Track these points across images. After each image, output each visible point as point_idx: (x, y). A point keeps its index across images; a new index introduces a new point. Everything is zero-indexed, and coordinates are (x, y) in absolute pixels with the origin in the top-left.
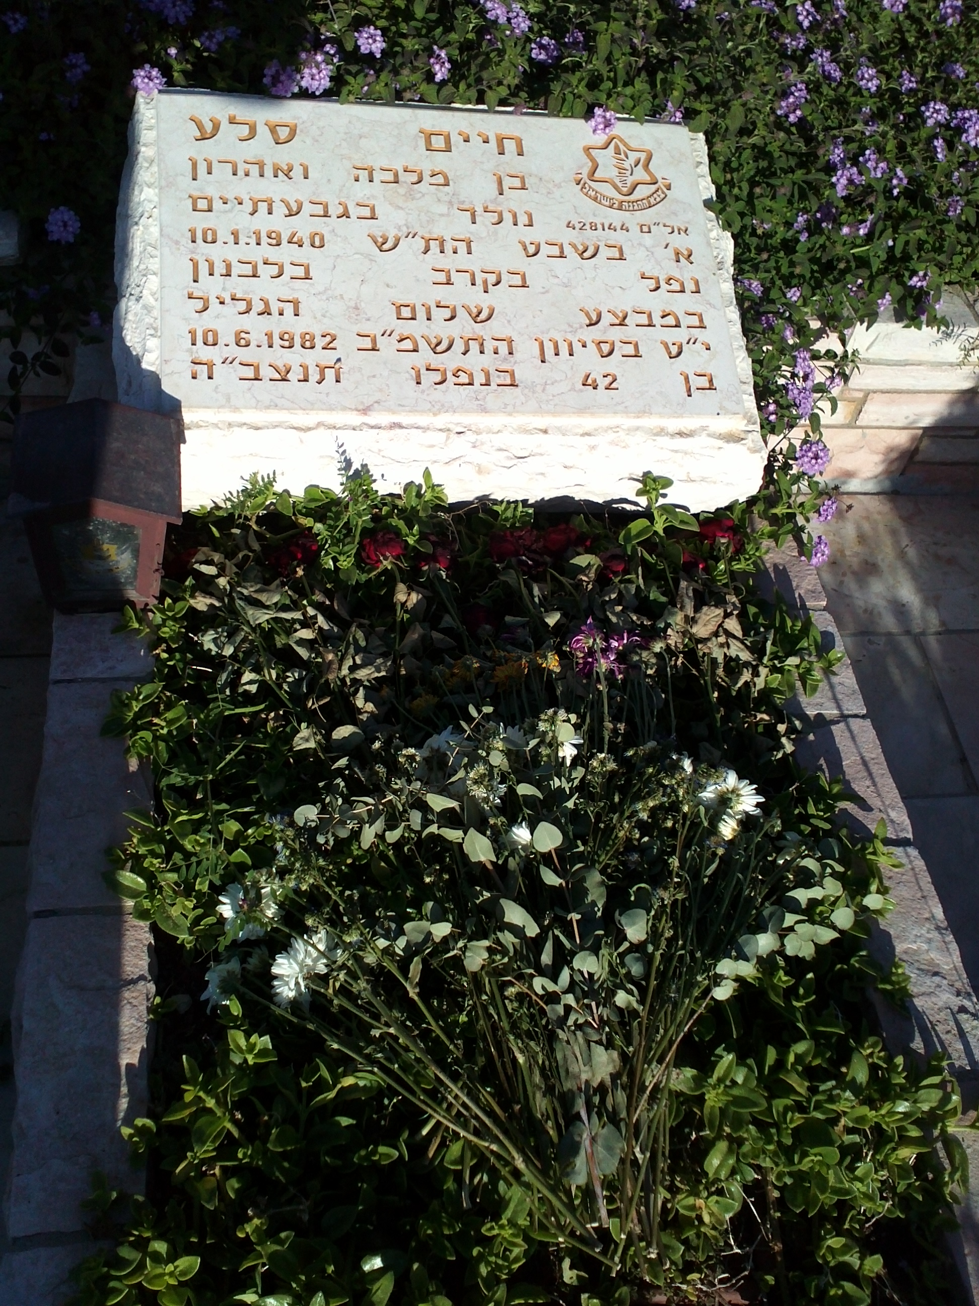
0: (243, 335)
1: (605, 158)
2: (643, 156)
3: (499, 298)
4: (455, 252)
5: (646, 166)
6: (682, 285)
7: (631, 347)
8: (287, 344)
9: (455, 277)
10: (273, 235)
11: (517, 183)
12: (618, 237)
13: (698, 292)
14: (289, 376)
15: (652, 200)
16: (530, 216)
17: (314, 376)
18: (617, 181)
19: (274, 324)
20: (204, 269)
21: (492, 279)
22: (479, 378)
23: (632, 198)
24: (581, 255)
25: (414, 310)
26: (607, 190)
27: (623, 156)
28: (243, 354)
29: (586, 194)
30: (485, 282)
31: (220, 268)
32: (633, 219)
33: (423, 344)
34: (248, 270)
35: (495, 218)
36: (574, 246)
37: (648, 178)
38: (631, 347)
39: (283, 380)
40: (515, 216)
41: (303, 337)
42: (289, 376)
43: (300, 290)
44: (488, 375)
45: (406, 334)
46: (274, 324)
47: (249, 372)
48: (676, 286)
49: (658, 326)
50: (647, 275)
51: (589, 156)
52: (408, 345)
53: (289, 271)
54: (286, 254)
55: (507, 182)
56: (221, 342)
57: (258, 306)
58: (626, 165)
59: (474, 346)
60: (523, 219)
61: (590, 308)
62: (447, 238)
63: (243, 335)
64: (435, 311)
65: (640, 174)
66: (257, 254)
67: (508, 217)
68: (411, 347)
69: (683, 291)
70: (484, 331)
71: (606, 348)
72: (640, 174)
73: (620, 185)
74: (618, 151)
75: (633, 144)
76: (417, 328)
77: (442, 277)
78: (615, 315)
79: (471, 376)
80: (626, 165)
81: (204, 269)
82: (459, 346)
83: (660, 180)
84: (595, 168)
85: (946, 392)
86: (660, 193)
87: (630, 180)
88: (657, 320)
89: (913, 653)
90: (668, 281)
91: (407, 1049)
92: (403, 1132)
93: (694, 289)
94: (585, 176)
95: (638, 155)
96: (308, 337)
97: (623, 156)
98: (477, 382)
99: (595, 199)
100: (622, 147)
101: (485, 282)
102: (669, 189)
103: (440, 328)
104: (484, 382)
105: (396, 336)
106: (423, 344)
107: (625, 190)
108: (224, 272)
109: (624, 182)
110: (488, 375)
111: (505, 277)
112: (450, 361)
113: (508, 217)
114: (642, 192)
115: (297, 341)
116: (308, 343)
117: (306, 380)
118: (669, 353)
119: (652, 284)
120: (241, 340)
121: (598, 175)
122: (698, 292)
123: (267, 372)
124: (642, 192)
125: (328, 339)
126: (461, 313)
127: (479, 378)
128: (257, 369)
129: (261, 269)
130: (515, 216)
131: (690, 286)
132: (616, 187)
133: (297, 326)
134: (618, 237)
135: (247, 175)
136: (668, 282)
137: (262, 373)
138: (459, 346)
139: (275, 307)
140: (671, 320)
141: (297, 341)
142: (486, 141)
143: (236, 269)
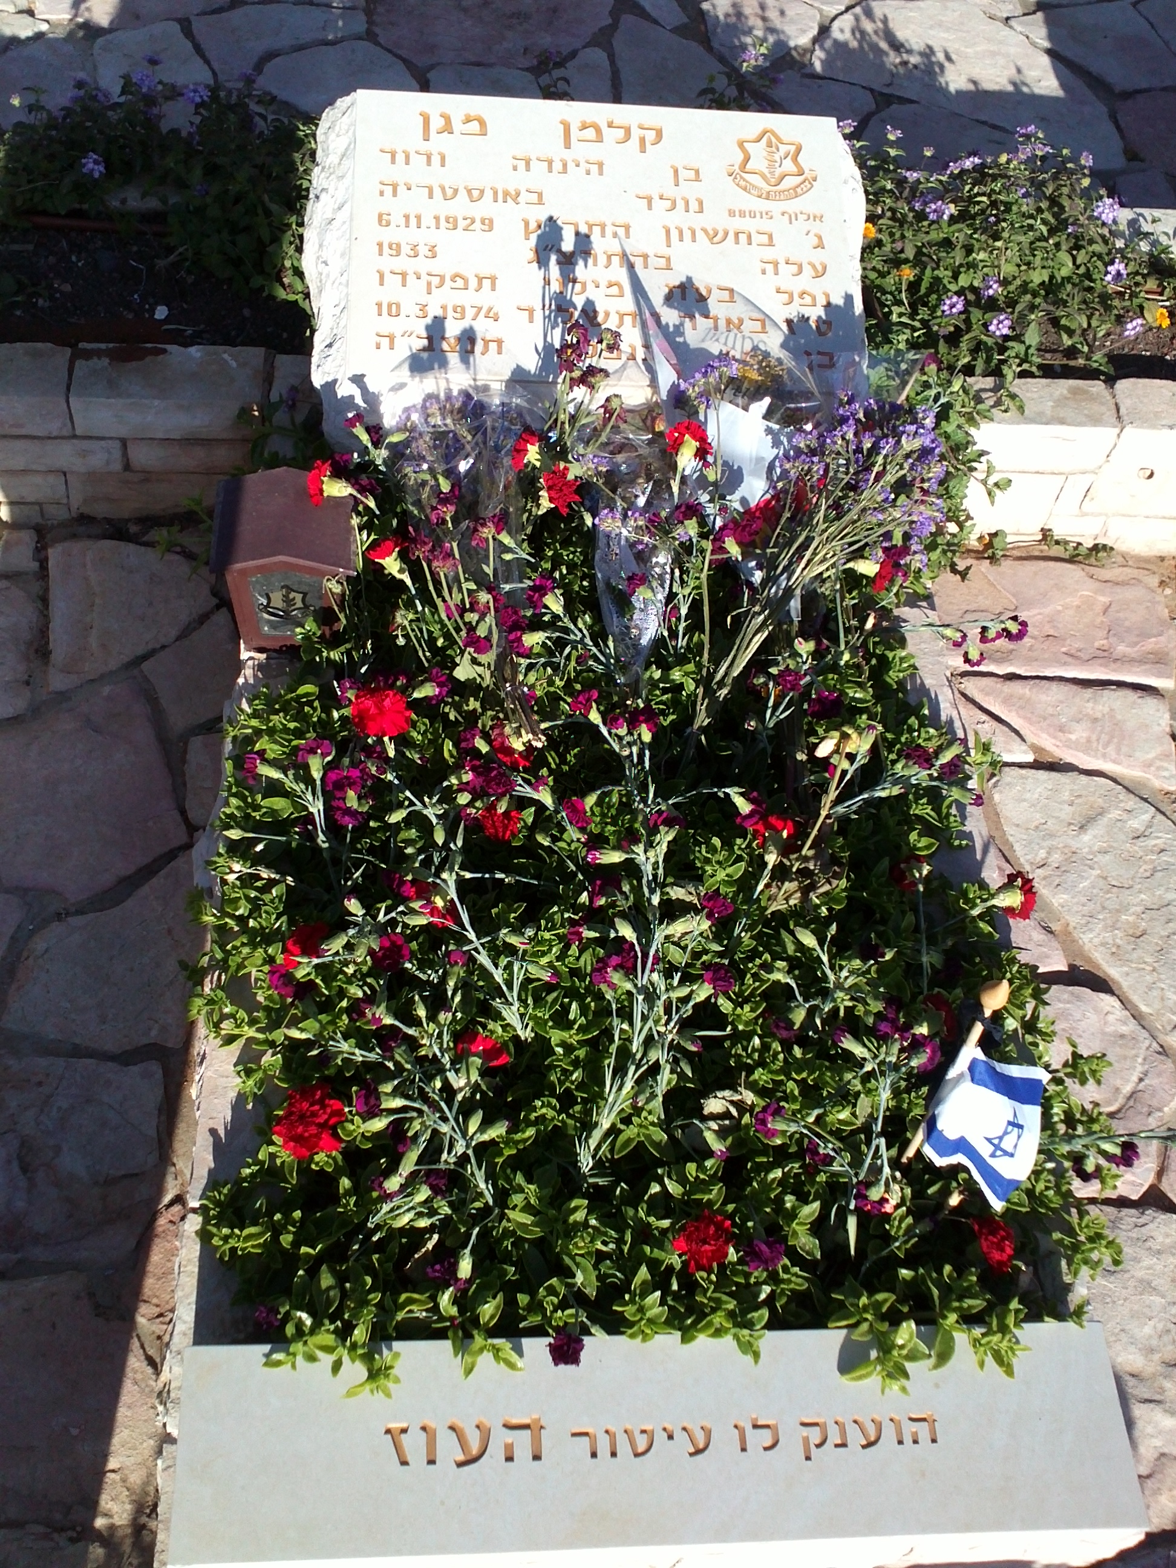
1: (758, 151)
2: (793, 148)
5: (795, 160)
8: (458, 316)
12: (766, 225)
15: (799, 190)
16: (701, 203)
18: (766, 171)
24: (711, 239)
32: (776, 207)
35: (668, 204)
36: (705, 231)
40: (687, 203)
41: (390, 306)
55: (683, 174)
56: (403, 313)
58: (777, 157)
60: (694, 206)
67: (680, 204)
72: (788, 166)
74: (769, 144)
75: (785, 139)
80: (777, 157)
83: (807, 171)
84: (747, 159)
85: (403, 362)
87: (778, 172)
90: (802, 295)
91: (59, 1109)
92: (1059, 1265)
94: (736, 167)
99: (745, 189)
100: (773, 140)
113: (680, 204)
114: (789, 182)
121: (749, 167)
124: (789, 182)
130: (687, 203)
134: (766, 225)
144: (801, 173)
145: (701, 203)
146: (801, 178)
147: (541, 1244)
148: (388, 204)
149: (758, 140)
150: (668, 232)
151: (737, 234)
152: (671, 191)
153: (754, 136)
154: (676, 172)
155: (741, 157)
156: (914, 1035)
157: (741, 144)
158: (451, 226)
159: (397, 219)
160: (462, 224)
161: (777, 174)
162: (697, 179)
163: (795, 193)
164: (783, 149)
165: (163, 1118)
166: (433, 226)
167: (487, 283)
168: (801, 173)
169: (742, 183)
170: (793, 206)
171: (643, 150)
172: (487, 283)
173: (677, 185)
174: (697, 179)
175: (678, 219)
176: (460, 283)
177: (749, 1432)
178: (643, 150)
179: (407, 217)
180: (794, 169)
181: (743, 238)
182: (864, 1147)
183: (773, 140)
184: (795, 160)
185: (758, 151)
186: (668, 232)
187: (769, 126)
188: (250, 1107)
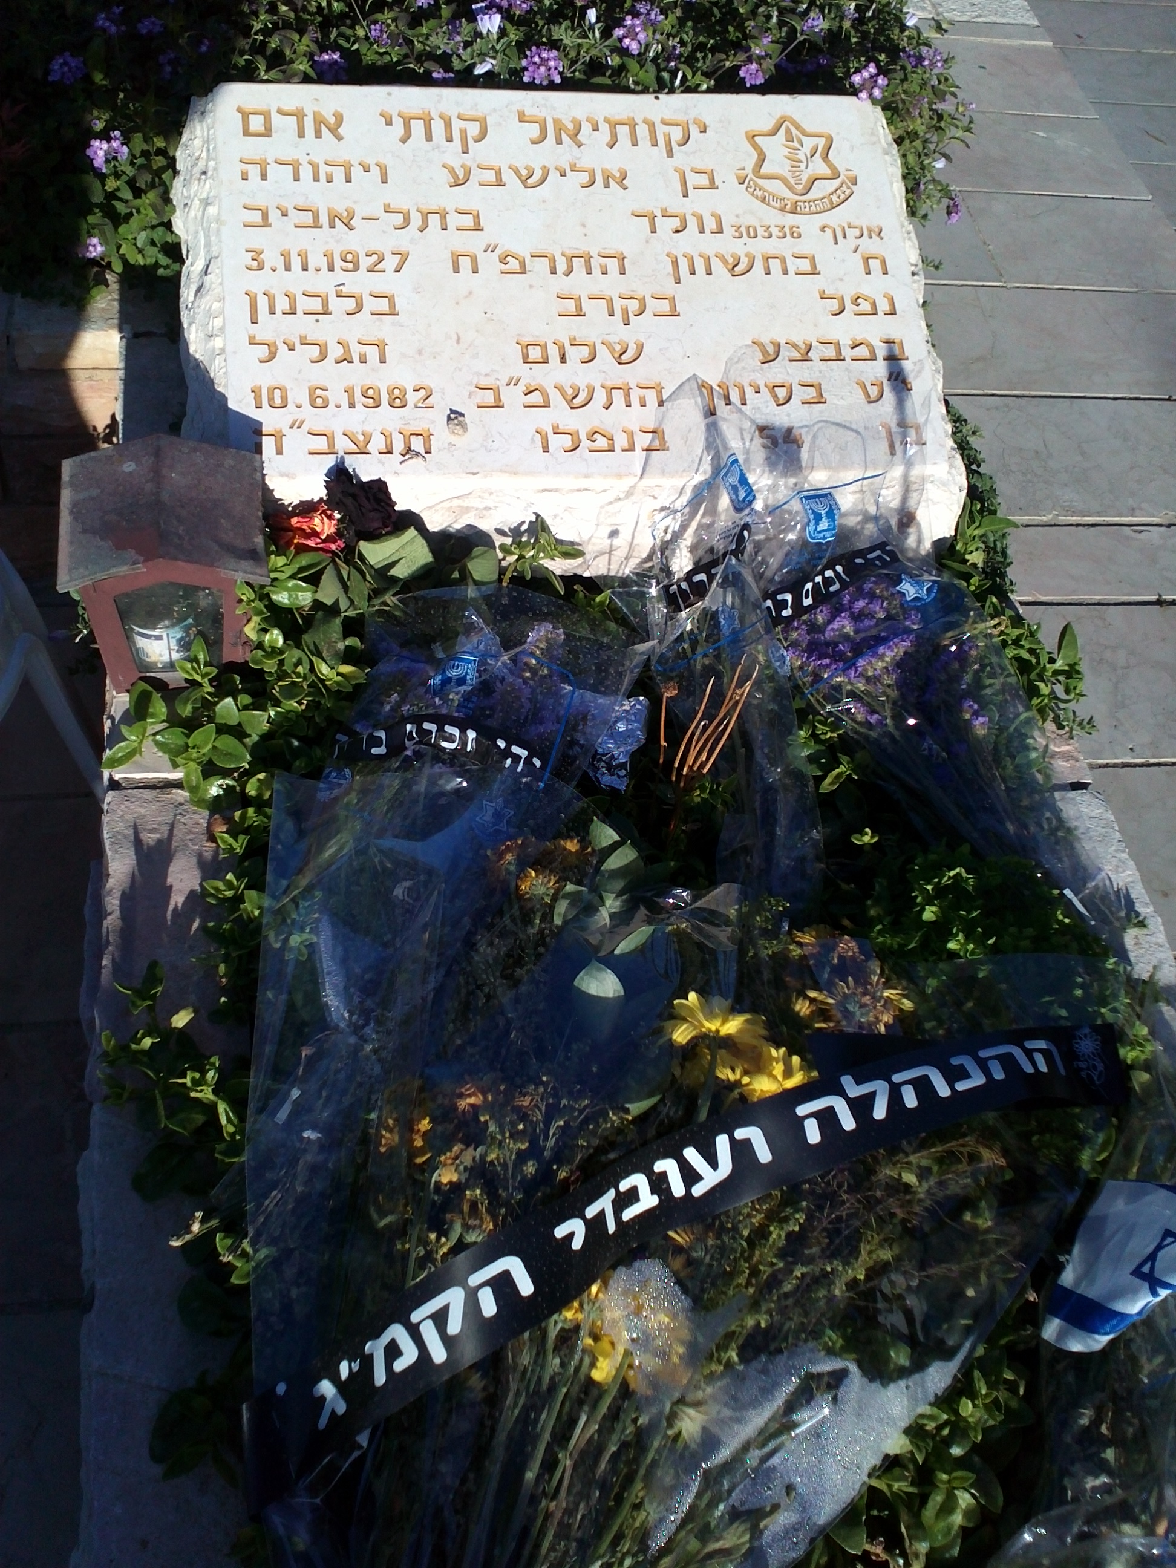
0: (319, 392)
2: (821, 142)
3: (644, 328)
4: (605, 273)
5: (825, 157)
6: (874, 304)
9: (586, 305)
10: (349, 257)
11: (704, 180)
19: (356, 375)
20: (263, 303)
21: (634, 306)
22: (621, 441)
23: (810, 196)
25: (544, 348)
26: (775, 187)
27: (796, 144)
28: (316, 419)
29: (753, 194)
30: (625, 311)
31: (282, 304)
32: (809, 224)
33: (555, 397)
34: (316, 304)
37: (827, 172)
41: (390, 392)
43: (384, 329)
44: (631, 435)
46: (356, 375)
48: (865, 306)
49: (848, 359)
50: (828, 293)
51: (755, 146)
52: (536, 398)
53: (370, 304)
54: (360, 282)
55: (692, 180)
57: (336, 352)
59: (618, 396)
60: (710, 224)
61: (765, 339)
62: (594, 254)
63: (319, 392)
64: (571, 352)
65: (819, 167)
66: (325, 283)
67: (692, 224)
70: (631, 375)
71: (782, 393)
72: (819, 167)
73: (792, 181)
74: (790, 138)
75: (809, 128)
76: (552, 375)
77: (570, 305)
78: (795, 346)
81: (263, 303)
82: (600, 397)
83: (842, 170)
84: (762, 159)
86: (844, 188)
88: (847, 352)
89: (389, 815)
90: (856, 301)
94: (749, 170)
95: (816, 140)
96: (397, 392)
97: (796, 144)
98: (617, 448)
99: (763, 200)
100: (793, 129)
101: (625, 311)
102: (855, 184)
103: (575, 374)
104: (626, 446)
105: (521, 387)
106: (555, 397)
107: (799, 188)
108: (287, 308)
109: (798, 179)
110: (631, 435)
111: (651, 303)
112: (592, 416)
113: (692, 224)
114: (821, 189)
115: (385, 398)
116: (398, 401)
118: (867, 395)
119: (835, 305)
120: (317, 399)
121: (764, 170)
124: (821, 189)
125: (422, 393)
126: (603, 352)
129: (334, 303)
131: (883, 306)
133: (384, 379)
135: (330, 180)
136: (856, 301)
138: (600, 397)
139: (356, 350)
140: (862, 351)
141: (385, 398)
143: (303, 304)
144: (836, 175)
146: (836, 183)
147: (693, 1455)
148: (258, 238)
149: (774, 132)
150: (675, 263)
151: (766, 259)
152: (677, 204)
153: (768, 126)
157: (752, 137)
158: (350, 266)
159: (272, 258)
160: (365, 262)
161: (805, 178)
162: (713, 186)
164: (809, 143)
165: (761, 1439)
166: (281, 267)
168: (836, 175)
169: (759, 193)
171: (670, 154)
173: (686, 196)
174: (713, 186)
175: (691, 243)
178: (670, 154)
179: (286, 256)
180: (827, 172)
181: (775, 265)
183: (793, 129)
184: (825, 157)
185: (775, 148)
186: (675, 263)
188: (176, 1243)
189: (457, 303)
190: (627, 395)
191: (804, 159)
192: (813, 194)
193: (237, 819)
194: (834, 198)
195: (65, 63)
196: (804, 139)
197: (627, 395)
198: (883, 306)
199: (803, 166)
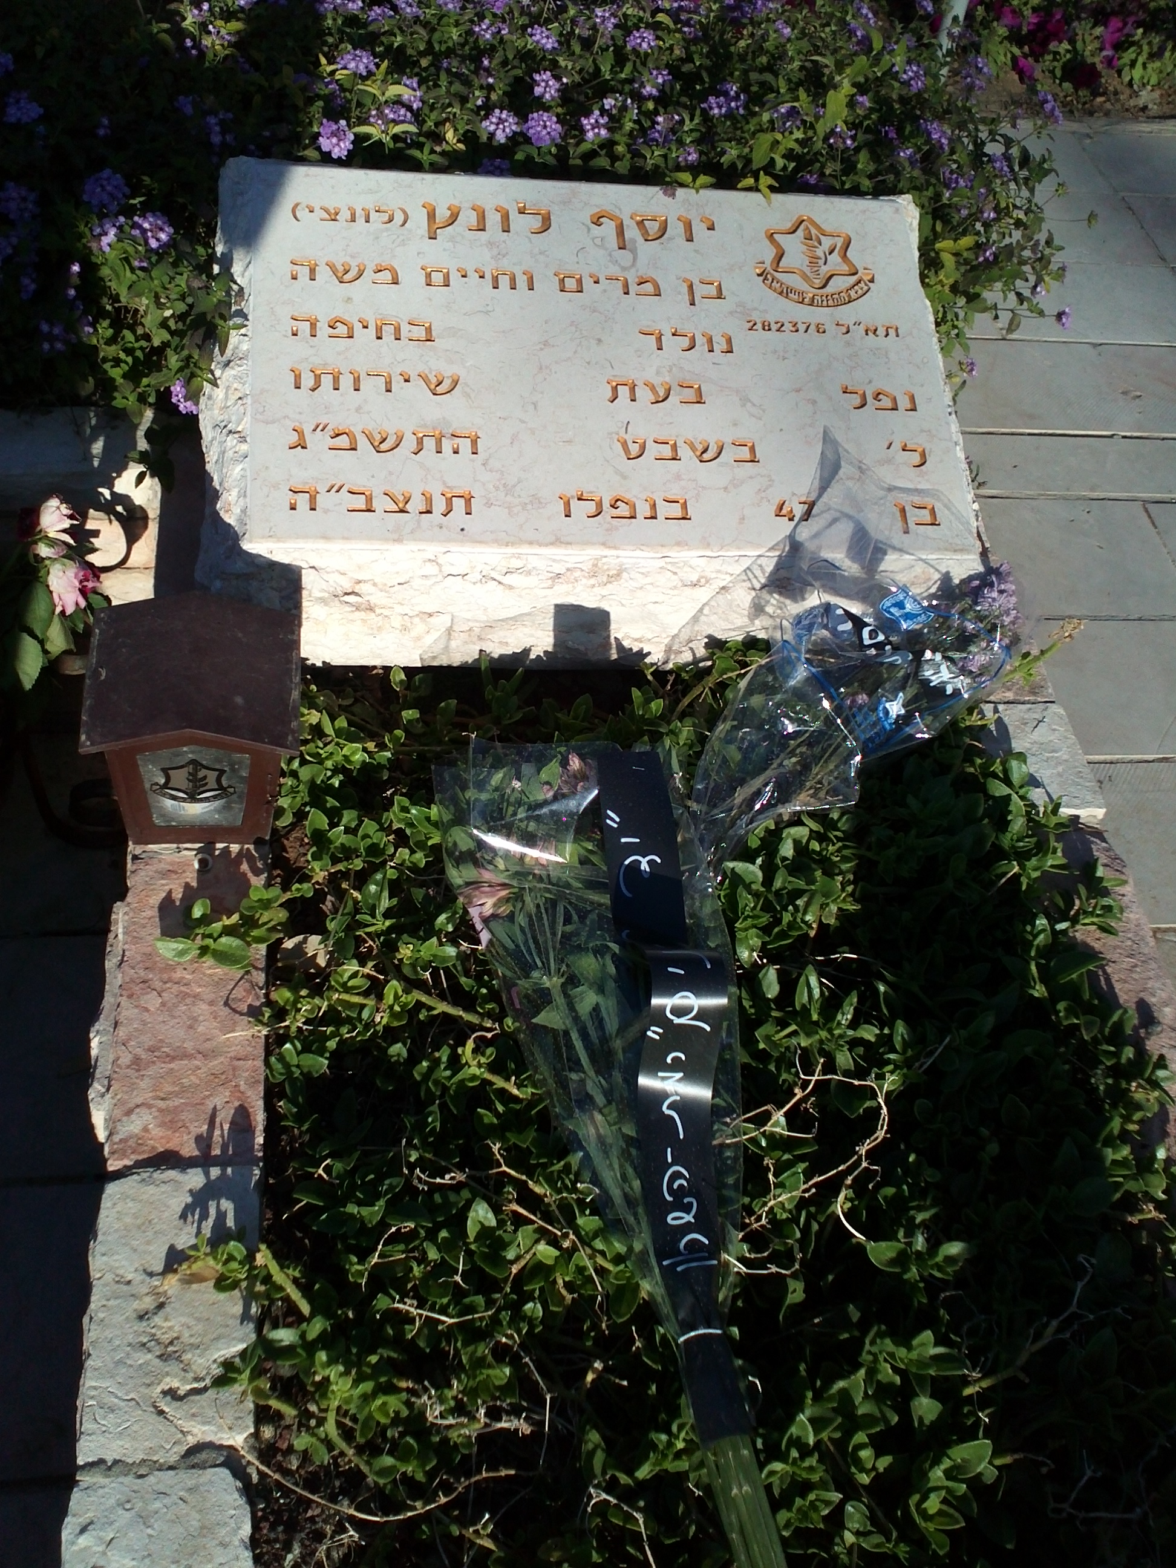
1: (793, 246)
2: (840, 242)
5: (844, 256)
7: (926, 512)
13: (914, 409)
14: (408, 507)
15: (852, 293)
17: (439, 505)
18: (807, 270)
22: (643, 510)
26: (794, 281)
35: (685, 342)
38: (926, 512)
39: (402, 511)
40: (710, 341)
42: (408, 507)
45: (341, 429)
47: (360, 502)
48: (886, 402)
52: (343, 441)
55: (700, 290)
58: (819, 252)
67: (700, 341)
68: (347, 445)
69: (895, 409)
79: (633, 507)
80: (819, 252)
82: (410, 442)
84: (780, 256)
86: (862, 284)
87: (825, 270)
90: (877, 396)
93: (909, 406)
94: (768, 265)
100: (814, 231)
105: (329, 431)
106: (363, 443)
113: (700, 341)
114: (838, 284)
117: (654, 517)
122: (914, 409)
123: (381, 503)
124: (838, 284)
127: (643, 510)
128: (369, 499)
130: (710, 341)
132: (805, 277)
137: (375, 505)
142: (482, 277)
145: (729, 341)
146: (854, 279)
153: (788, 225)
154: (691, 287)
155: (769, 254)
156: (878, 1382)
157: (771, 237)
163: (845, 299)
167: (459, 504)
170: (847, 314)
172: (459, 504)
176: (342, 329)
177: (514, 215)
182: (435, 1012)
184: (844, 256)
185: (793, 246)
187: (805, 213)
189: (293, 508)
190: (439, 443)
191: (822, 255)
192: (829, 289)
193: (101, 490)
194: (852, 293)
195: (24, 199)
196: (822, 238)
197: (439, 443)
198: (903, 403)
199: (821, 262)
